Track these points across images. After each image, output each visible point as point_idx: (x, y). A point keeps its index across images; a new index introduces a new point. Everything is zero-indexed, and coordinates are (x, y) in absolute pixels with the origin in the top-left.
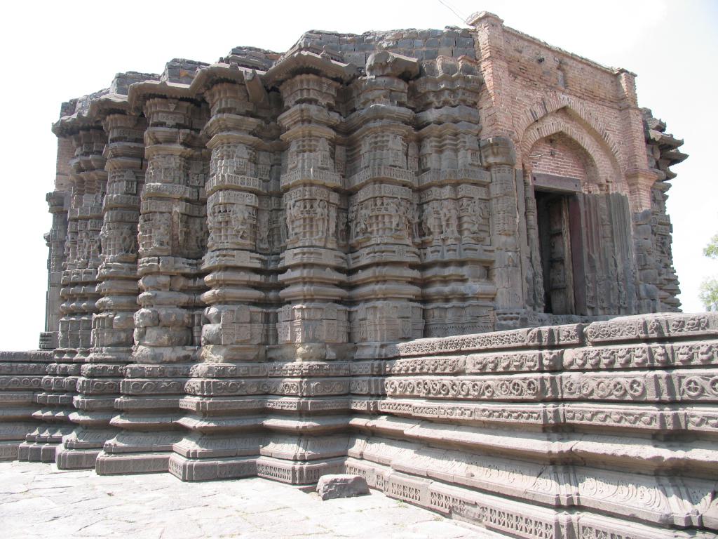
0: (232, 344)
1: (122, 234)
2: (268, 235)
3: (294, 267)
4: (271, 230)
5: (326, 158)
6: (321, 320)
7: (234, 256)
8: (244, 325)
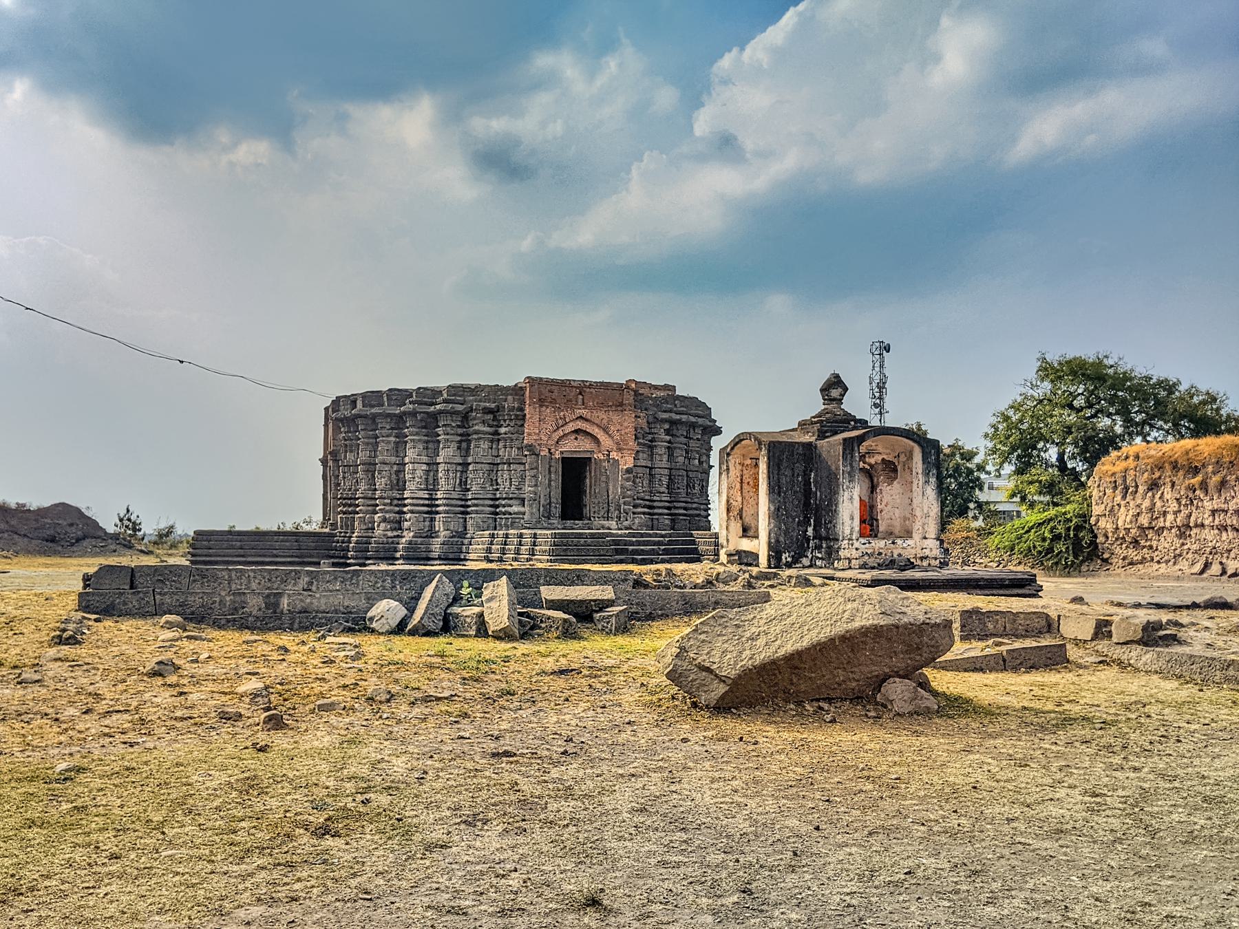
2: (431, 485)
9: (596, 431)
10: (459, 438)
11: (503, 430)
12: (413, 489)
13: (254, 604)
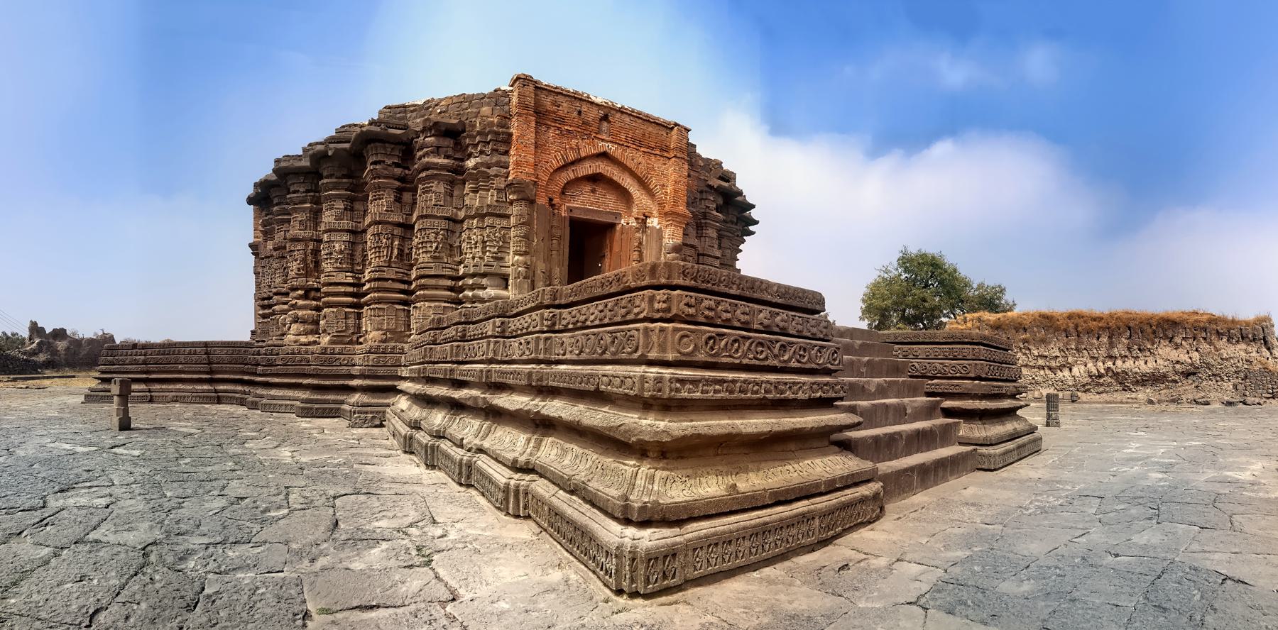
9: (628, 182)
10: (397, 184)
11: (470, 163)
13: (1228, 582)
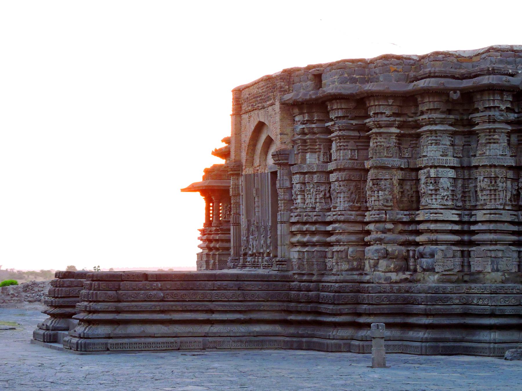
0: (442, 272)
1: (349, 190)
3: (482, 222)
4: (464, 192)
5: (505, 148)
6: (502, 257)
7: (442, 214)
8: (450, 259)
10: (510, 128)
12: (438, 207)
